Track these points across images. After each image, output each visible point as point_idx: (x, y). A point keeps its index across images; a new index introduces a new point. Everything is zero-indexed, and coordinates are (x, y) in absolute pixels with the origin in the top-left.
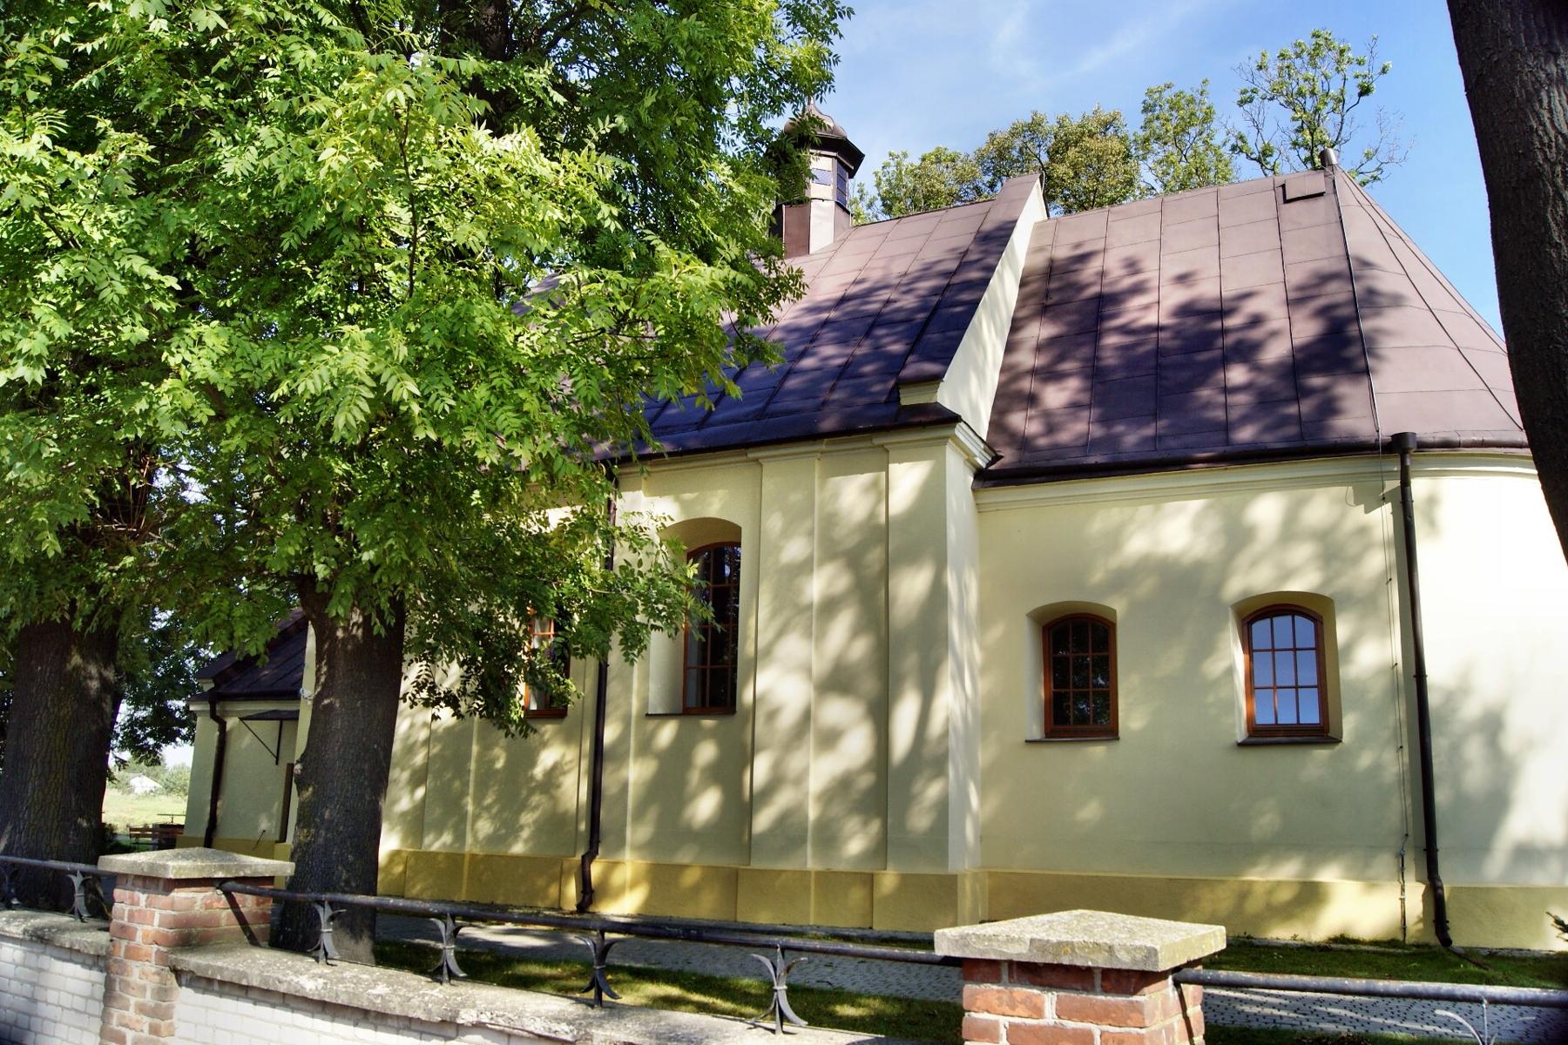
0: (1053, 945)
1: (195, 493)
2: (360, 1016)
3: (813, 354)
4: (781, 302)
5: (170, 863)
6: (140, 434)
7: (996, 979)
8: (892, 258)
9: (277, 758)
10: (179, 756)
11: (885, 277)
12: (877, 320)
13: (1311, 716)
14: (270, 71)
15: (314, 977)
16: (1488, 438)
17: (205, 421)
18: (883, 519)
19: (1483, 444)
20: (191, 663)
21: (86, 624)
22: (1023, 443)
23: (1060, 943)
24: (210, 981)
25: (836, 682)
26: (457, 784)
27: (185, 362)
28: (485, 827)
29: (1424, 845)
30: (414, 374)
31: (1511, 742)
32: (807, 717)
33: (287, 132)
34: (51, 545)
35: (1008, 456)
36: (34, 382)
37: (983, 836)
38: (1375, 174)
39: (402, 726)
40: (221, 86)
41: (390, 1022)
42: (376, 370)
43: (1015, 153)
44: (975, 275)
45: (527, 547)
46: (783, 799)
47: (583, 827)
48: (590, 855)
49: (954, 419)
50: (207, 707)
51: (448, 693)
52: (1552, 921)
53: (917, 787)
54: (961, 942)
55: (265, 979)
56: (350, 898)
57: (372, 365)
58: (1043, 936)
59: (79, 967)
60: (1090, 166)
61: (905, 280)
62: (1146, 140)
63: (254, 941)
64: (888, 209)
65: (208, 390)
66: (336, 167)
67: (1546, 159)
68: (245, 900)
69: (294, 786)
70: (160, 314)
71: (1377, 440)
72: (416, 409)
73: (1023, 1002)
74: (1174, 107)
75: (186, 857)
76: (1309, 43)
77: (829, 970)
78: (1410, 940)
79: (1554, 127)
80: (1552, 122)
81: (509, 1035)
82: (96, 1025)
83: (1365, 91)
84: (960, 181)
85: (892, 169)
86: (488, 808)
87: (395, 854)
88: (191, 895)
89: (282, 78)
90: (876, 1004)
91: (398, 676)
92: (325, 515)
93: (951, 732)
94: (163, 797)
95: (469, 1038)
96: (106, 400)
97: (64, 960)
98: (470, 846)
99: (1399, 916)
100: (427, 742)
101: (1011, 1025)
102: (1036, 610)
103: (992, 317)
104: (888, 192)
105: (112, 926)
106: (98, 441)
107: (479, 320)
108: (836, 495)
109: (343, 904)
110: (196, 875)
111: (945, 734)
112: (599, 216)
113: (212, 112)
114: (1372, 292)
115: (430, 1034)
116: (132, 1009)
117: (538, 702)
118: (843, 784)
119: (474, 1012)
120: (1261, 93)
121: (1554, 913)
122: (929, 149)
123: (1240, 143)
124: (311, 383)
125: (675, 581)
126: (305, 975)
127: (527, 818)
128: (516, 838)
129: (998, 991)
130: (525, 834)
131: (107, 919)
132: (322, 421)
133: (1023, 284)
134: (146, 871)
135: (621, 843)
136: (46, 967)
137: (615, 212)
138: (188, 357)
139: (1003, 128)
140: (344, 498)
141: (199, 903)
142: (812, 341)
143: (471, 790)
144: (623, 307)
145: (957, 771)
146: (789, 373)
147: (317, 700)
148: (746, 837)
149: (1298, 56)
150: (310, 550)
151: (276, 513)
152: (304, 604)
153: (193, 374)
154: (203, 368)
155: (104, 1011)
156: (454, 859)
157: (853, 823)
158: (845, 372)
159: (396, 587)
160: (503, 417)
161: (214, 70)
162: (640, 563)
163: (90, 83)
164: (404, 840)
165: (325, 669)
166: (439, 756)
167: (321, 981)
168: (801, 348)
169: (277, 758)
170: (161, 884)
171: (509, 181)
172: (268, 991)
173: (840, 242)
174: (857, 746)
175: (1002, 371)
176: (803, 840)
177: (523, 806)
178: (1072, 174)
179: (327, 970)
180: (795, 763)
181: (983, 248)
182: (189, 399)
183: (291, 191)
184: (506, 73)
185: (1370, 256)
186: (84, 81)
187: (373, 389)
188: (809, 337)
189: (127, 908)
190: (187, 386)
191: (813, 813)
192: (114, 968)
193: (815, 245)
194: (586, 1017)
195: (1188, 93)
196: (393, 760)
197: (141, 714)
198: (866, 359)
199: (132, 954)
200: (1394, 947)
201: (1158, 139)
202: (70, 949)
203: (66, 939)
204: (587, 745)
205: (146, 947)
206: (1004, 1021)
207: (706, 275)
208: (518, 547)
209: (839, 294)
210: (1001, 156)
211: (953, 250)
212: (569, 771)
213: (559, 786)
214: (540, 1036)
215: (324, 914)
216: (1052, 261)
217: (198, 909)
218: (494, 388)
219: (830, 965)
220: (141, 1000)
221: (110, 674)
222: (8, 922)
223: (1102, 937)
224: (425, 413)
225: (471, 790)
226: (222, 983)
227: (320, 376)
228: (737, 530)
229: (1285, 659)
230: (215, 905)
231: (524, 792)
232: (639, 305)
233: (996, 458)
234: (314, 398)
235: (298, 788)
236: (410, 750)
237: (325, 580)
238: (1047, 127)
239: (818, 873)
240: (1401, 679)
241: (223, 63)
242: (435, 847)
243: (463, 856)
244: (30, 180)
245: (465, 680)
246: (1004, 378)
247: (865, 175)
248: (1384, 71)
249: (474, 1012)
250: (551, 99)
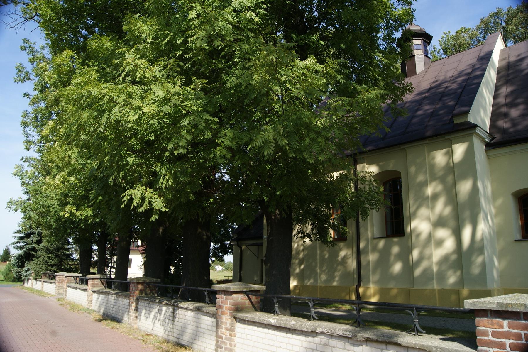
0: (505, 304)
1: (227, 177)
2: (288, 330)
3: (421, 110)
4: (405, 95)
5: (231, 287)
6: (213, 164)
7: (486, 316)
8: (447, 71)
9: (258, 257)
10: (229, 258)
11: (445, 78)
12: (444, 94)
14: (237, 53)
15: (274, 319)
17: (230, 157)
18: (452, 164)
20: (230, 230)
21: (202, 219)
22: (504, 131)
23: (507, 304)
24: (245, 320)
25: (440, 223)
26: (314, 264)
27: (222, 142)
28: (324, 277)
30: (286, 138)
32: (430, 236)
33: (243, 70)
34: (192, 197)
35: (498, 137)
36: (184, 153)
37: (500, 276)
39: (295, 246)
40: (223, 61)
41: (297, 332)
42: (275, 137)
43: (492, 24)
44: (478, 73)
45: (327, 186)
46: (424, 264)
47: (356, 276)
48: (359, 285)
50: (236, 243)
51: (308, 234)
53: (473, 258)
54: (473, 304)
55: (260, 320)
56: (282, 296)
57: (274, 136)
58: (501, 301)
59: (208, 317)
60: (523, 23)
61: (452, 78)
63: (256, 310)
64: (445, 53)
65: (229, 148)
66: (257, 80)
68: (252, 297)
69: (264, 264)
70: (215, 129)
72: (288, 148)
73: (496, 324)
75: (235, 285)
77: (443, 322)
81: (332, 336)
82: (214, 334)
84: (471, 38)
86: (324, 271)
87: (295, 287)
88: (237, 296)
89: (240, 54)
90: (460, 333)
91: (292, 230)
92: (266, 181)
93: (484, 238)
94: (225, 272)
95: (320, 336)
96: (202, 155)
97: (204, 315)
98: (319, 283)
100: (303, 250)
101: (492, 331)
103: (487, 87)
104: (444, 47)
105: (217, 305)
106: (201, 167)
107: (304, 119)
108: (434, 158)
109: (281, 298)
110: (238, 290)
111: (482, 239)
112: (338, 79)
113: (222, 68)
115: (308, 336)
116: (224, 329)
117: (337, 235)
118: (445, 259)
119: (321, 329)
122: (458, 28)
124: (257, 143)
125: (377, 193)
126: (272, 319)
127: (337, 274)
128: (334, 281)
129: (487, 320)
130: (337, 279)
131: (215, 303)
132: (261, 155)
134: (225, 289)
135: (369, 282)
136: (200, 317)
137: (343, 77)
138: (223, 140)
139: (486, 16)
140: (270, 176)
141: (240, 298)
142: (420, 105)
143: (318, 265)
144: (348, 108)
145: (488, 252)
146: (413, 117)
147: (268, 238)
148: (412, 278)
150: (262, 193)
151: (251, 183)
152: (262, 209)
153: (225, 145)
154: (227, 143)
155: (216, 330)
156: (314, 288)
157: (450, 272)
158: (432, 115)
159: (288, 202)
160: (314, 148)
161: (221, 56)
162: (365, 188)
163: (189, 66)
164: (298, 282)
165: (269, 228)
166: (307, 254)
167: (276, 320)
168: (417, 108)
169: (258, 257)
170: (522, 316)
171: (309, 74)
172: (261, 323)
173: (427, 68)
174: (449, 244)
175: (493, 106)
176: (433, 279)
177: (335, 270)
178: (515, 28)
179: (277, 317)
180: (427, 252)
181: (481, 63)
182: (225, 152)
183: (246, 88)
184: (305, 38)
186: (187, 66)
187: (274, 143)
188: (419, 103)
189: (220, 300)
190: (224, 148)
191: (435, 269)
192: (218, 317)
193: (418, 71)
194: (355, 330)
196: (293, 257)
197: (217, 246)
198: (441, 109)
199: (223, 313)
202: (206, 312)
203: (205, 309)
204: (355, 249)
205: (226, 311)
206: (490, 330)
207: (374, 93)
208: (325, 186)
209: (428, 87)
210: (486, 26)
211: (470, 65)
212: (350, 258)
213: (346, 263)
214: (341, 336)
215: (275, 301)
216: (509, 63)
217: (240, 300)
218: (311, 138)
219: (444, 321)
220: (226, 326)
221: (209, 234)
222: (189, 305)
223: (522, 302)
224: (291, 148)
225: (318, 265)
226: (248, 321)
227: (260, 141)
228: (399, 173)
230: (244, 299)
231: (335, 265)
232: (353, 107)
233: (493, 138)
234: (259, 148)
235: (265, 265)
236: (298, 253)
237: (267, 201)
238: (503, 12)
239: (439, 290)
241: (223, 53)
242: (309, 284)
243: (317, 286)
244: (178, 98)
245: (312, 230)
246: (494, 109)
247: (435, 42)
249: (321, 329)
250: (320, 43)
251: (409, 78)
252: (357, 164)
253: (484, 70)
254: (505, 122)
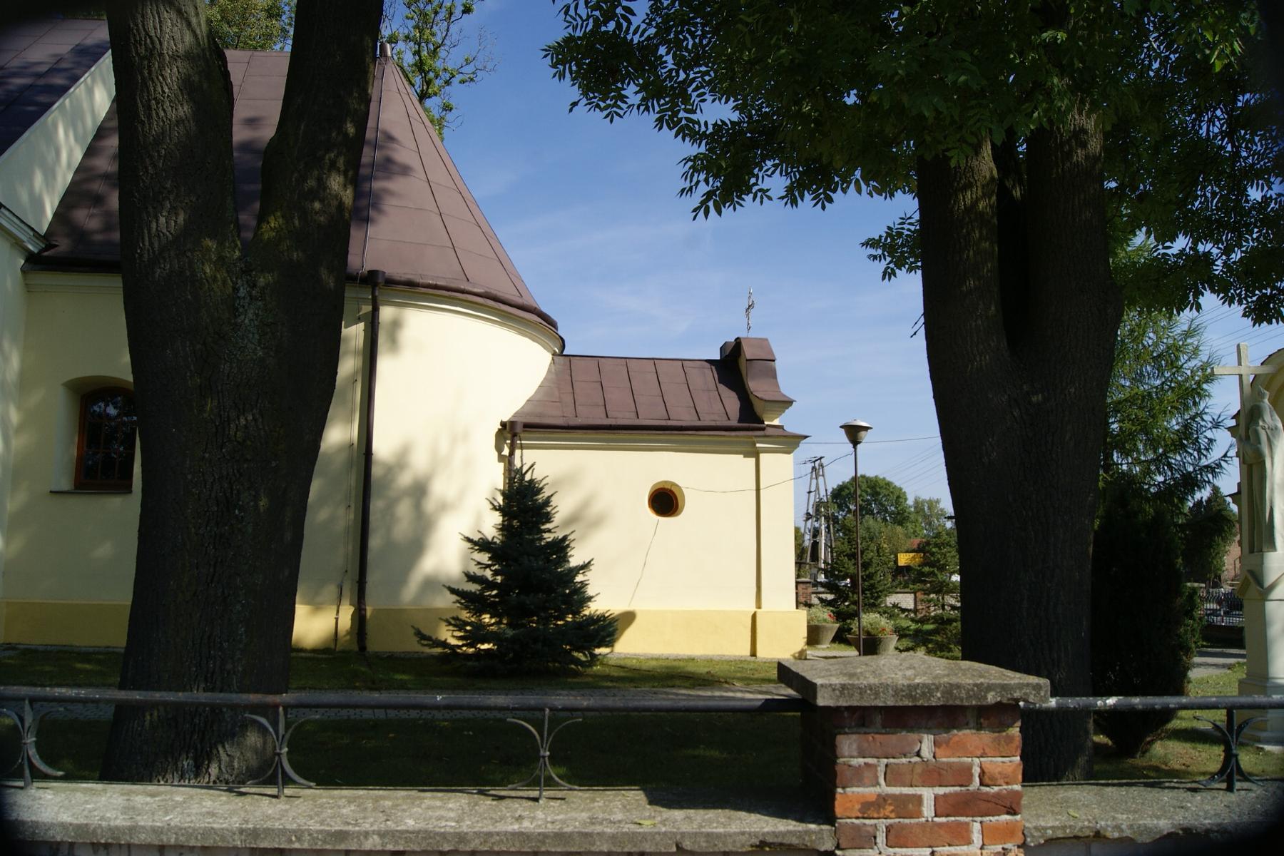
19: (436, 287)
22: (80, 235)
29: (357, 578)
31: (430, 505)
35: (64, 245)
38: (472, 76)
44: (59, 81)
67: (137, 54)
78: (339, 648)
79: (145, 30)
80: (143, 25)
83: (467, 10)
99: (334, 631)
102: (72, 380)
114: (389, 160)
170: (878, 719)
185: (396, 133)
233: (50, 246)
240: (355, 454)
246: (78, 178)
253: (75, 79)
254: (92, 216)
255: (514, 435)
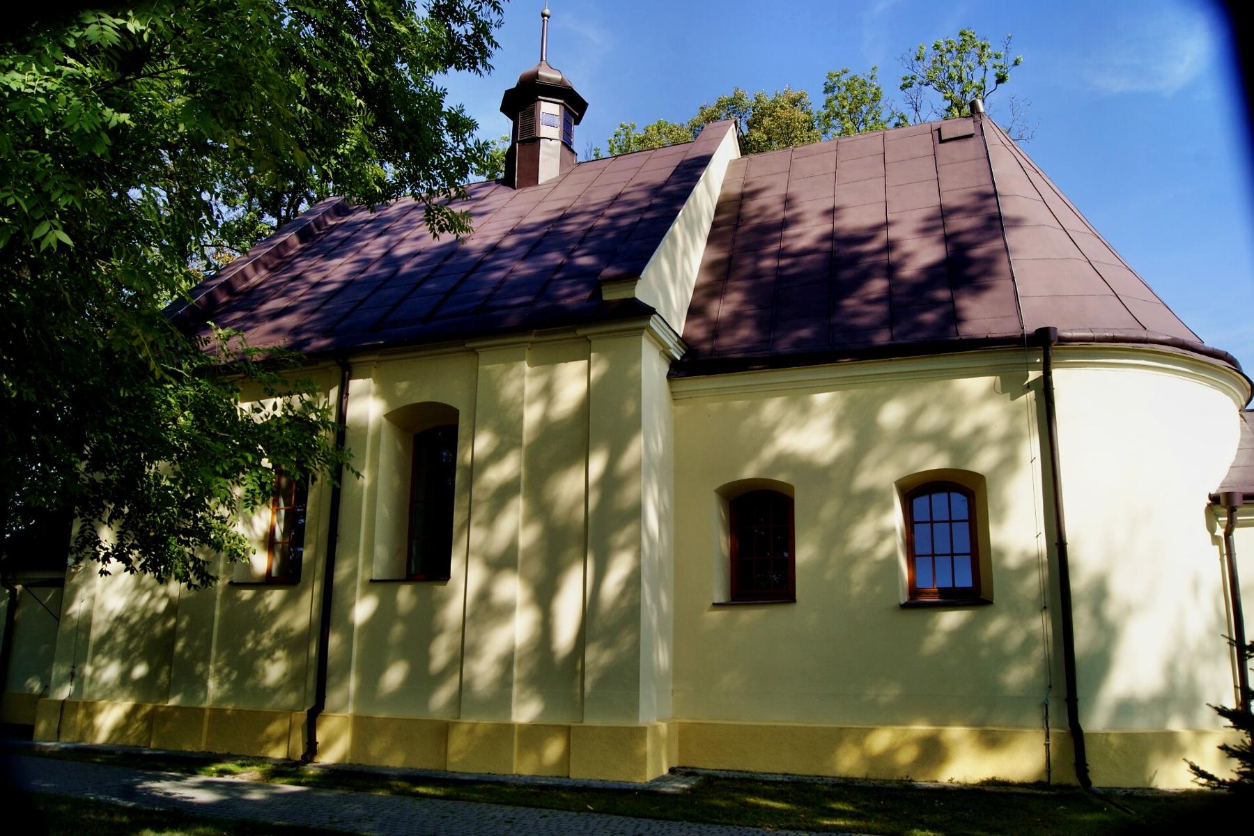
13: (964, 580)
16: (1118, 334)
19: (1114, 340)
29: (1065, 695)
31: (1112, 610)
49: (651, 311)
52: (1187, 766)
62: (828, 116)
71: (1023, 335)
74: (849, 88)
76: (956, 40)
83: (1001, 80)
85: (622, 137)
102: (724, 486)
120: (919, 79)
121: (1190, 760)
123: (902, 122)
133: (718, 211)
148: (579, 666)
149: (949, 51)
195: (861, 78)
200: (1040, 789)
201: (837, 114)
228: (454, 413)
229: (941, 530)
248: (1016, 63)
251: (518, 191)
252: (350, 378)
255: (1232, 511)
